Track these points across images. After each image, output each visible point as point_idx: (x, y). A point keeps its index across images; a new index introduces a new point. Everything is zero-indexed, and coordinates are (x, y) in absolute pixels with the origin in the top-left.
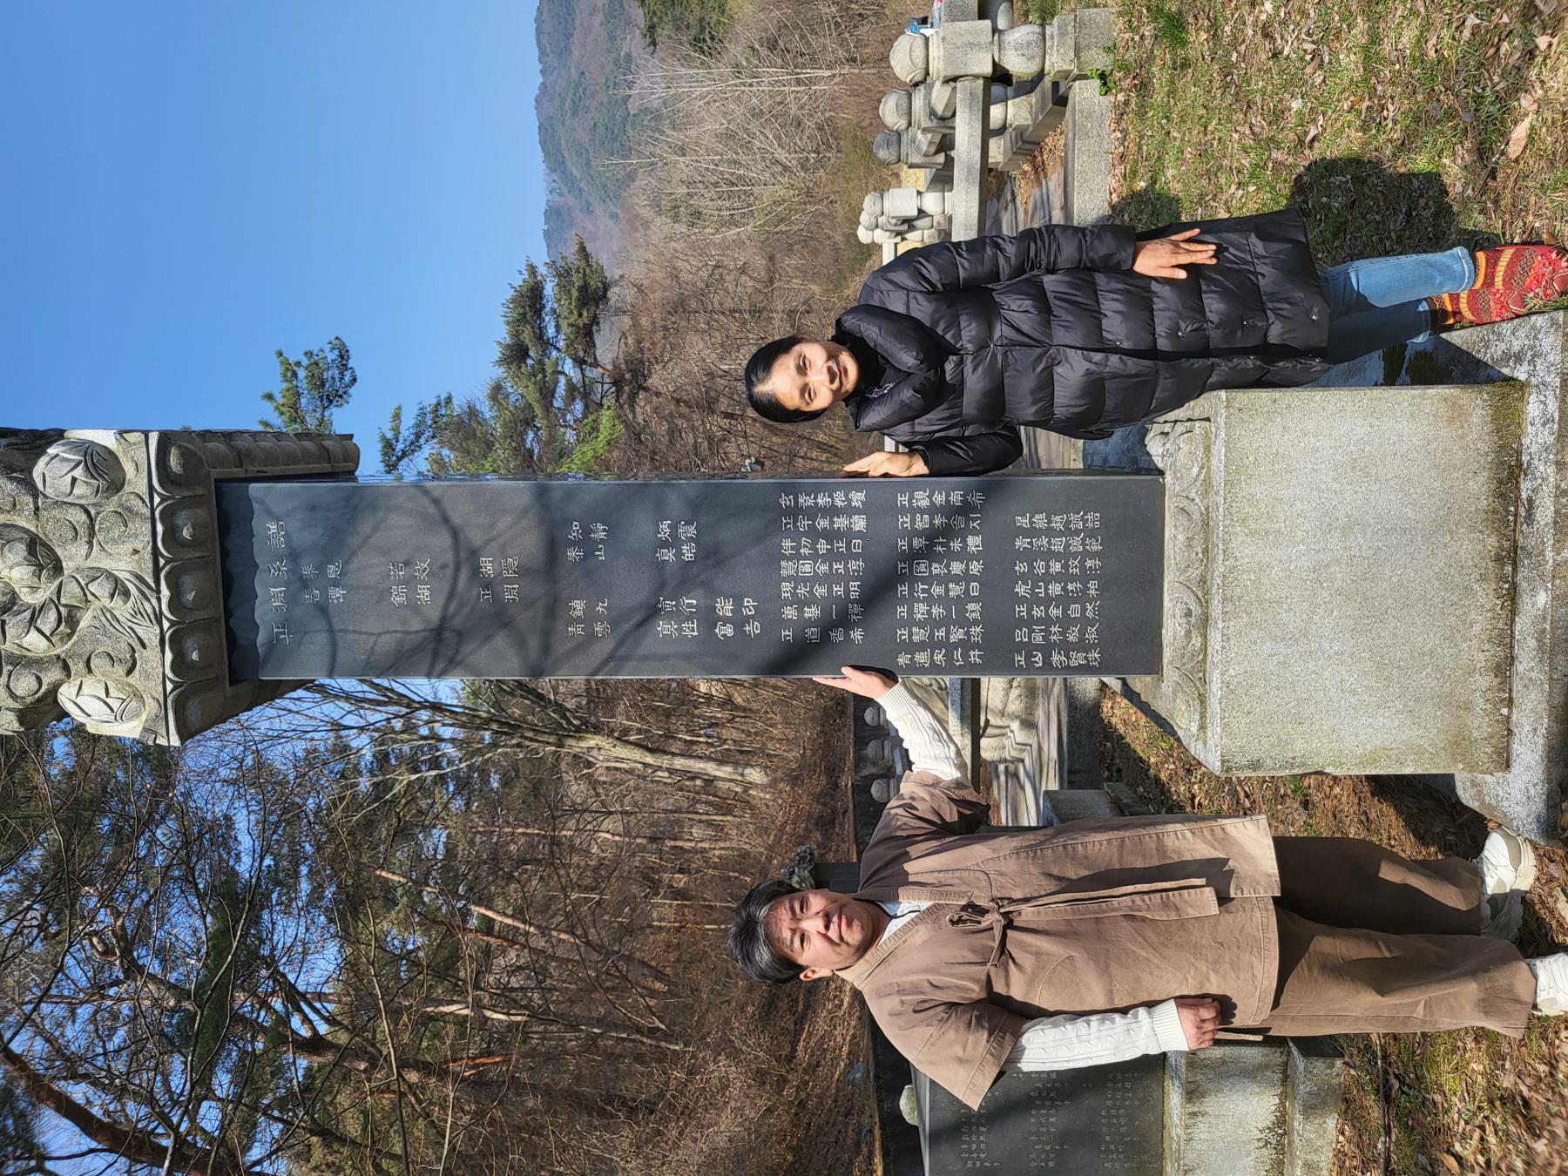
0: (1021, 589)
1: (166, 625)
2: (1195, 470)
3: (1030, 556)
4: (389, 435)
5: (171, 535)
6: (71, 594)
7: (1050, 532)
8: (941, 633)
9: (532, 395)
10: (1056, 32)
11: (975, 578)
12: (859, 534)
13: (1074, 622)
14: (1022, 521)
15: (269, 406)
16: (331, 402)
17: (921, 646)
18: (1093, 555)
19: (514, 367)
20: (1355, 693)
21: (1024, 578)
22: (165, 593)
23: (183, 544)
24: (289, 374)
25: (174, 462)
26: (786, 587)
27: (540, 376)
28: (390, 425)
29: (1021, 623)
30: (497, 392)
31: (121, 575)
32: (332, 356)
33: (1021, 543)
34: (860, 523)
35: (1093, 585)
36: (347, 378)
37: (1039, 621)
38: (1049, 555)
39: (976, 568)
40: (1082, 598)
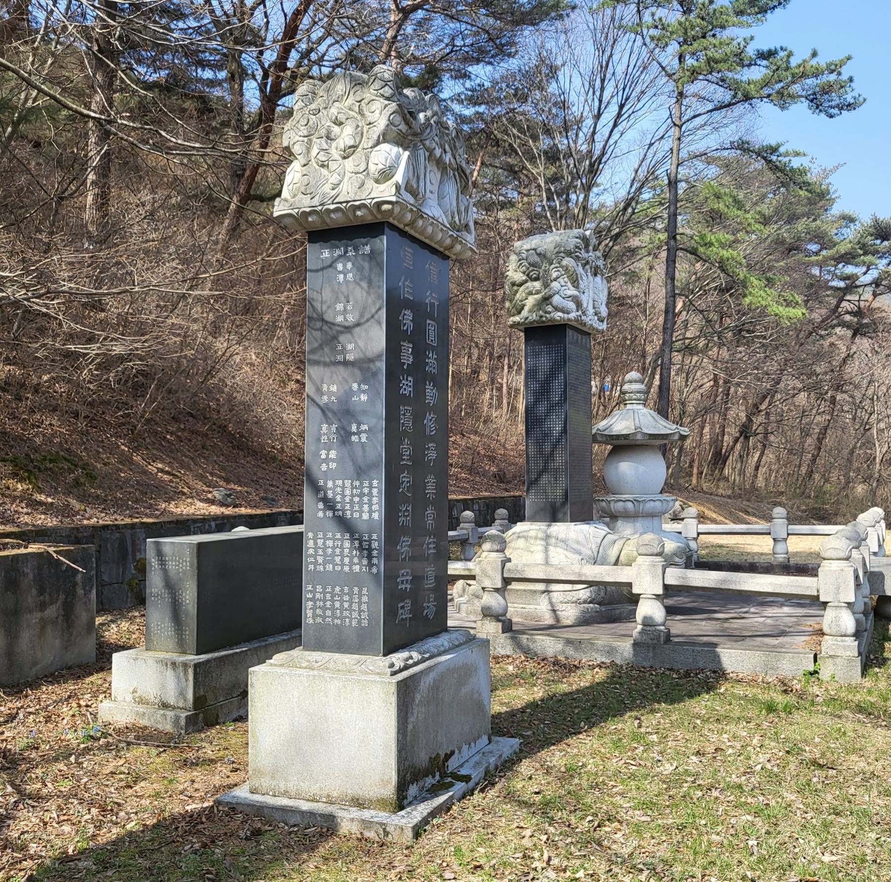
0: (338, 589)
1: (320, 208)
2: (371, 668)
3: (350, 594)
4: (782, 150)
5: (359, 207)
6: (333, 166)
7: (360, 603)
8: (320, 552)
9: (843, 249)
10: (846, 644)
11: (342, 568)
12: (361, 516)
13: (324, 613)
14: (365, 591)
15: (807, 55)
16: (812, 101)
17: (316, 543)
18: (350, 622)
19: (872, 230)
20: (278, 730)
21: (342, 590)
22: (332, 207)
23: (354, 212)
24: (833, 67)
25: (386, 207)
26: (339, 482)
27: (861, 252)
28: (790, 150)
29: (324, 588)
30: (850, 219)
31: (341, 186)
32: (850, 99)
33: (356, 589)
34: (365, 516)
35: (338, 621)
36: (832, 111)
37: (325, 597)
38: (351, 603)
39: (346, 569)
40: (334, 616)
